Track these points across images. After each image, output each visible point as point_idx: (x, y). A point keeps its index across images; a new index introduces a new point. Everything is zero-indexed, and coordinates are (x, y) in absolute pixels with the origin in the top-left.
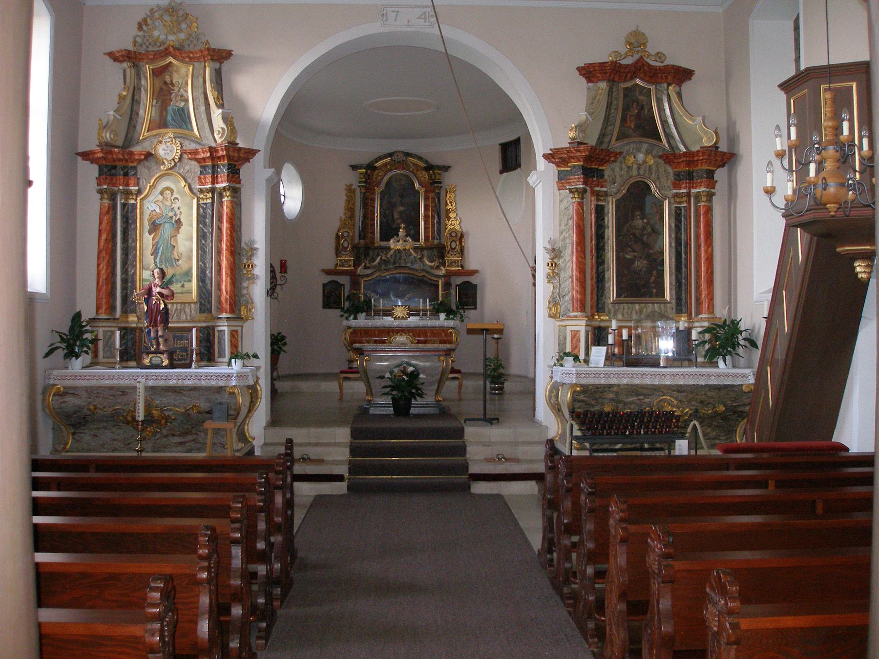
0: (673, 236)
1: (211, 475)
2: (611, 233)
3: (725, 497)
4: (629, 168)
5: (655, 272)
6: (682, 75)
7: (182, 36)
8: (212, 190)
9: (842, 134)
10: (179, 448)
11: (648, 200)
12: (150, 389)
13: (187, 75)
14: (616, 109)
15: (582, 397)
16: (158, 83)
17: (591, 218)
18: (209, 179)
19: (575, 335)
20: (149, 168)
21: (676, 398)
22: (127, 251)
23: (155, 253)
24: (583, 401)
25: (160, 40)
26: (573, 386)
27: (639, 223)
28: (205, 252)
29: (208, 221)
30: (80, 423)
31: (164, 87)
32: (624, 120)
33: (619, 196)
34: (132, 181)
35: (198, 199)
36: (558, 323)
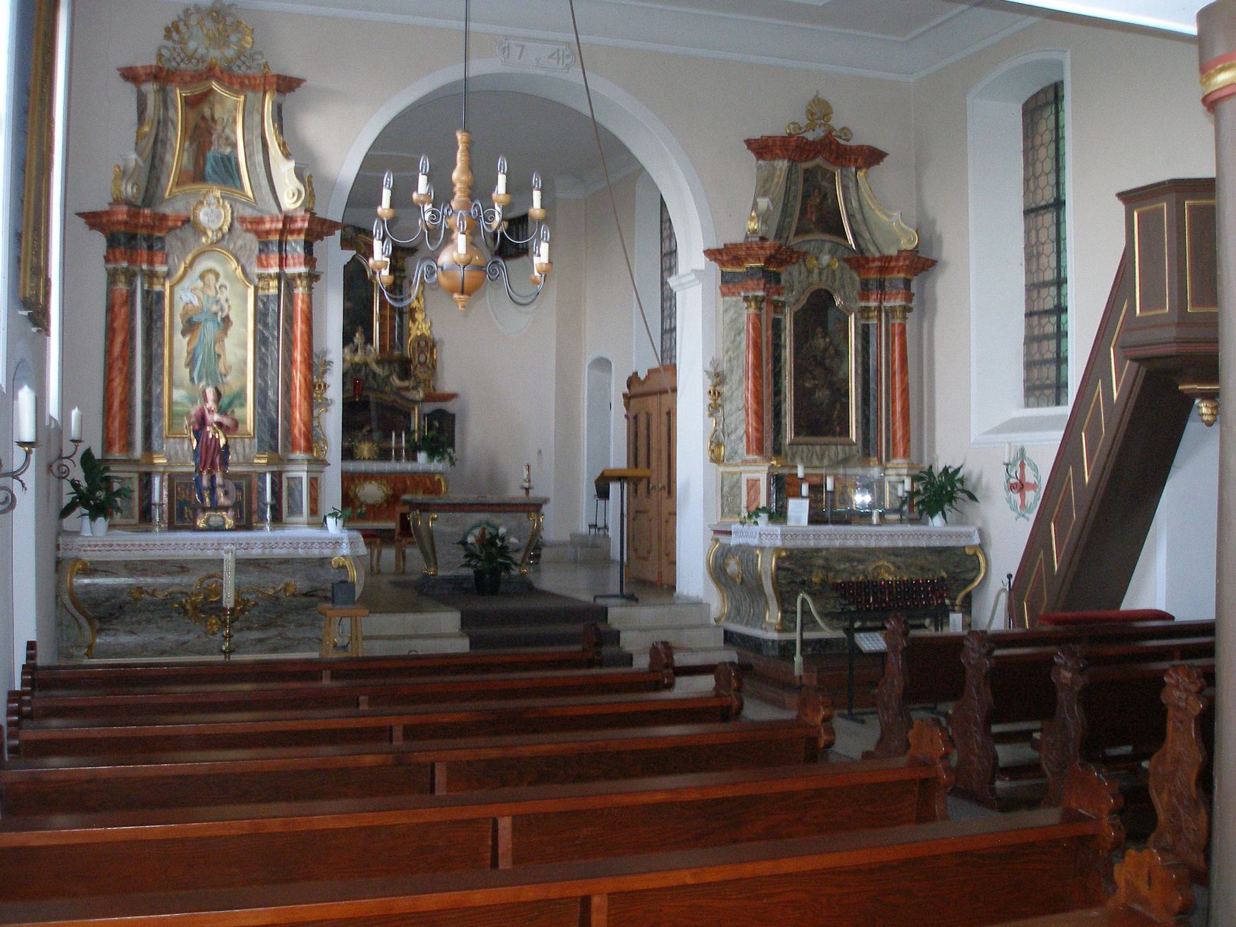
0: (860, 360)
1: (284, 685)
2: (788, 354)
3: (647, 701)
4: (810, 272)
5: (838, 406)
6: (873, 157)
7: (230, 52)
8: (279, 277)
9: (417, 190)
10: (259, 646)
11: (831, 314)
12: (243, 564)
13: (236, 110)
14: (795, 197)
15: (787, 564)
16: (193, 117)
17: (767, 335)
18: (274, 259)
19: (753, 485)
20: (183, 242)
21: (894, 564)
22: (151, 360)
23: (191, 363)
24: (788, 570)
25: (197, 55)
26: (777, 550)
27: (821, 342)
28: (266, 365)
29: (270, 320)
30: (111, 615)
31: (202, 125)
32: (803, 212)
33: (800, 306)
34: (158, 257)
35: (256, 289)
36: (721, 469)
